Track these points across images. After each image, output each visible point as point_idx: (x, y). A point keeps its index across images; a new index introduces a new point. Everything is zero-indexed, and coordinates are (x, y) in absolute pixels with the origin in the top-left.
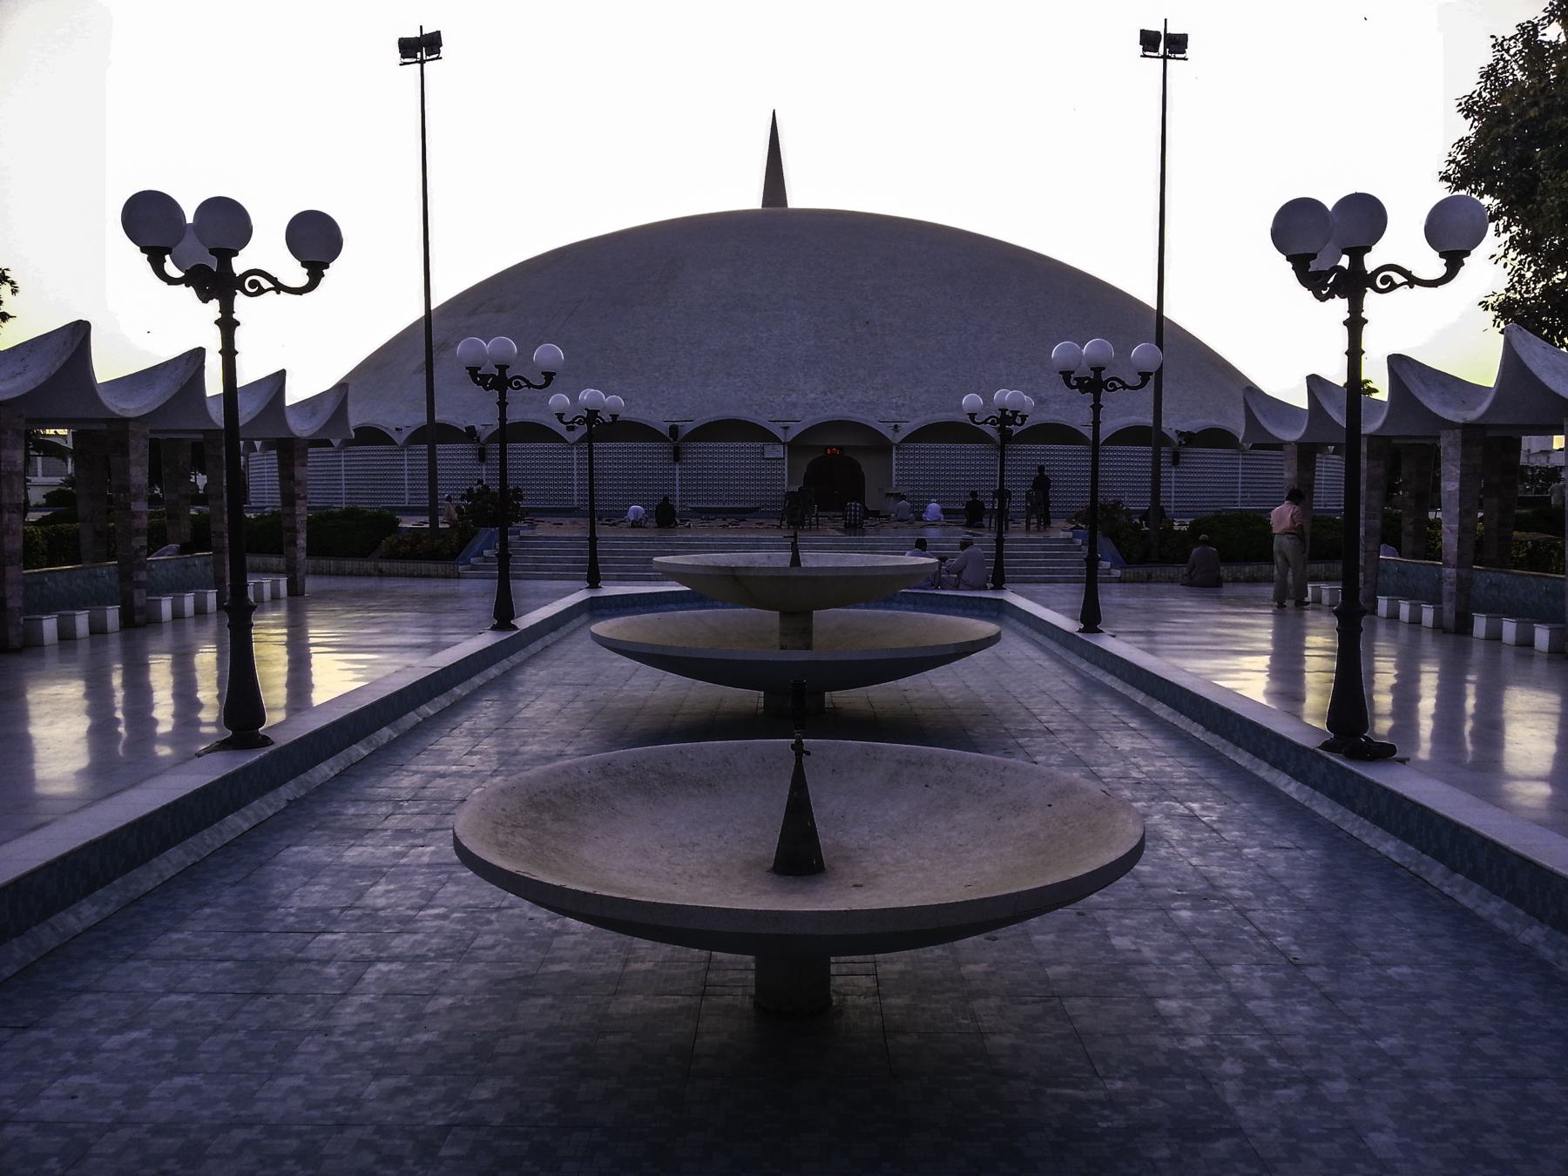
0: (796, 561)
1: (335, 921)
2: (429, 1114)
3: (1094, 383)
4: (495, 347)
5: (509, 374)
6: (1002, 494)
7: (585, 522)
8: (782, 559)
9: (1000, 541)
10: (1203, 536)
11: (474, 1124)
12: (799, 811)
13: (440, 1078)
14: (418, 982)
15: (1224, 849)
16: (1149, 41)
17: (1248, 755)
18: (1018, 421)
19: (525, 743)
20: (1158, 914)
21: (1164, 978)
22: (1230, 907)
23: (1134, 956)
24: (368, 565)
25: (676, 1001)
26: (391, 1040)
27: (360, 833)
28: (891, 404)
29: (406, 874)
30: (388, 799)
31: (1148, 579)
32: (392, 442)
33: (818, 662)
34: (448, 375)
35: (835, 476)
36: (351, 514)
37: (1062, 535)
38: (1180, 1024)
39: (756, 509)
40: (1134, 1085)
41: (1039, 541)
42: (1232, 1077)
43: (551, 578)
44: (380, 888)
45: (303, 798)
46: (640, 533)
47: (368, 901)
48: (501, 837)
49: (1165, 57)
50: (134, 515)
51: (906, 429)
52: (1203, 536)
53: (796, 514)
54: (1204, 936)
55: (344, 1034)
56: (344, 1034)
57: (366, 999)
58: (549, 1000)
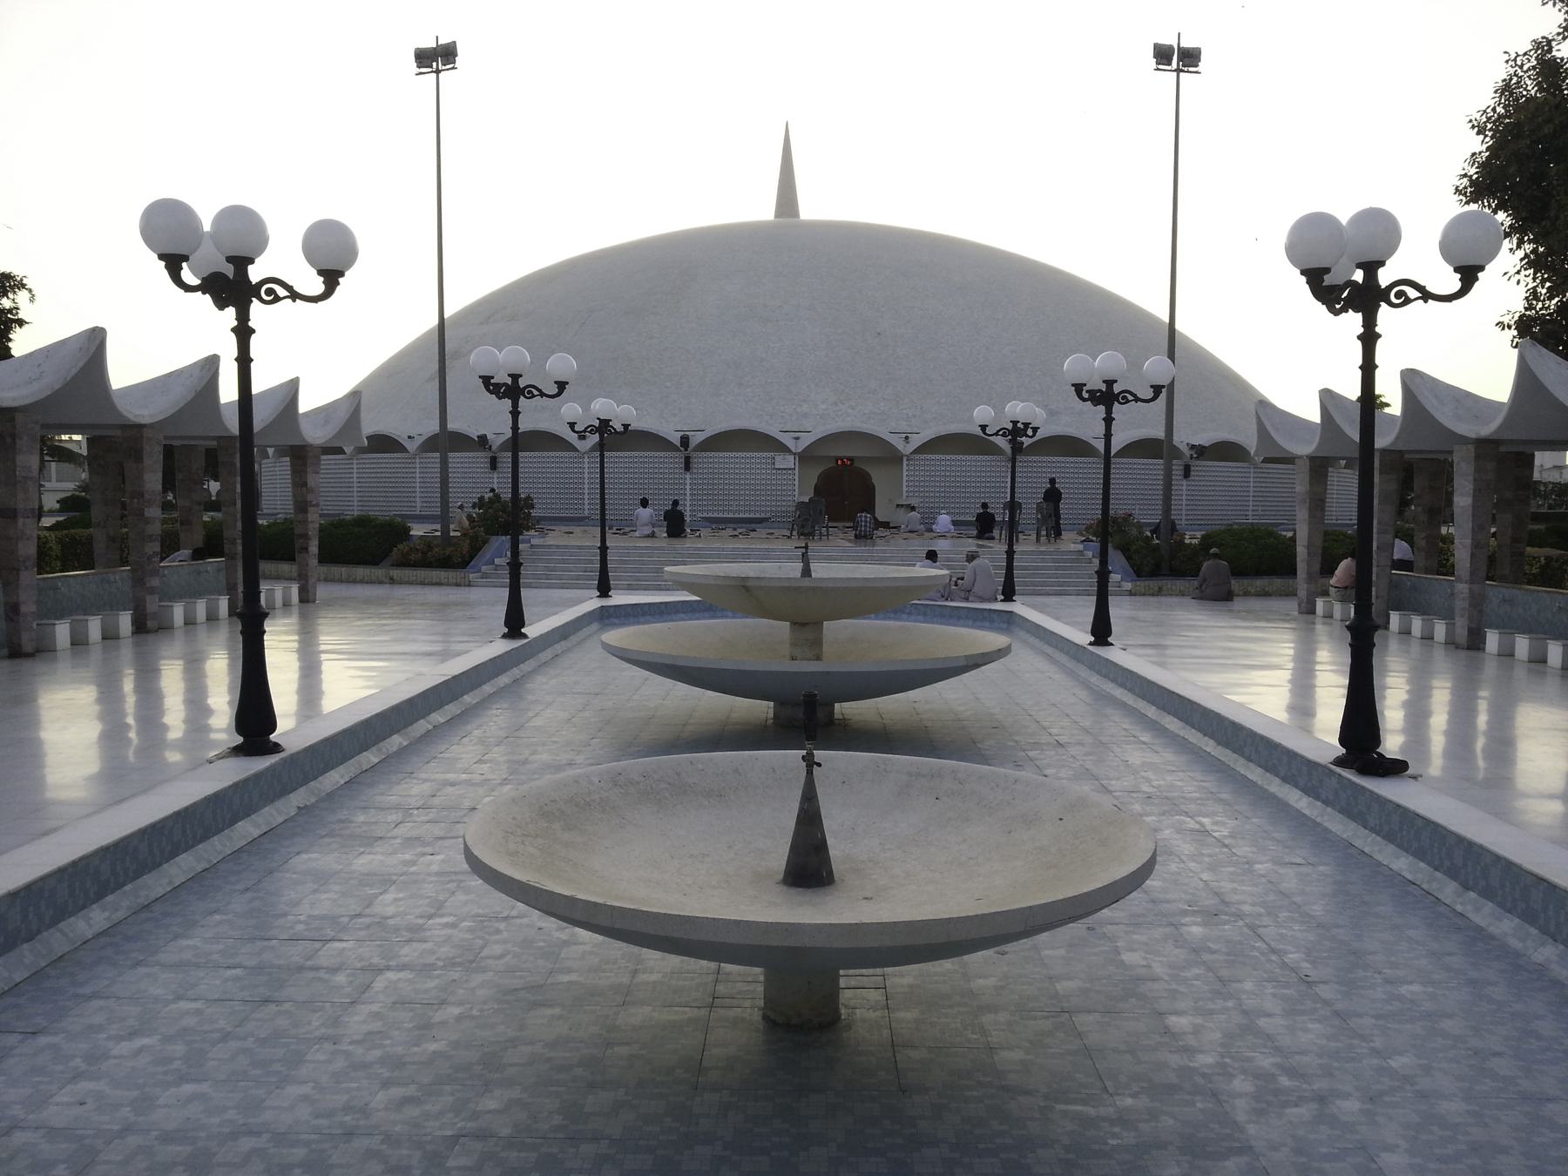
0: (806, 572)
4: (505, 359)
5: (522, 383)
6: (1013, 506)
8: (793, 569)
9: (1010, 554)
10: (1213, 550)
11: (481, 1135)
13: (448, 1088)
16: (1162, 55)
18: (1030, 432)
19: (535, 752)
22: (1241, 923)
23: (1142, 971)
24: (378, 572)
26: (400, 1050)
27: (370, 841)
29: (415, 882)
30: (397, 808)
32: (404, 450)
35: (842, 489)
36: (362, 522)
37: (1073, 547)
40: (1143, 1102)
42: (1240, 1095)
44: (389, 897)
45: (313, 805)
47: (377, 909)
49: (1178, 71)
52: (1213, 550)
57: (375, 1008)
58: (557, 1011)
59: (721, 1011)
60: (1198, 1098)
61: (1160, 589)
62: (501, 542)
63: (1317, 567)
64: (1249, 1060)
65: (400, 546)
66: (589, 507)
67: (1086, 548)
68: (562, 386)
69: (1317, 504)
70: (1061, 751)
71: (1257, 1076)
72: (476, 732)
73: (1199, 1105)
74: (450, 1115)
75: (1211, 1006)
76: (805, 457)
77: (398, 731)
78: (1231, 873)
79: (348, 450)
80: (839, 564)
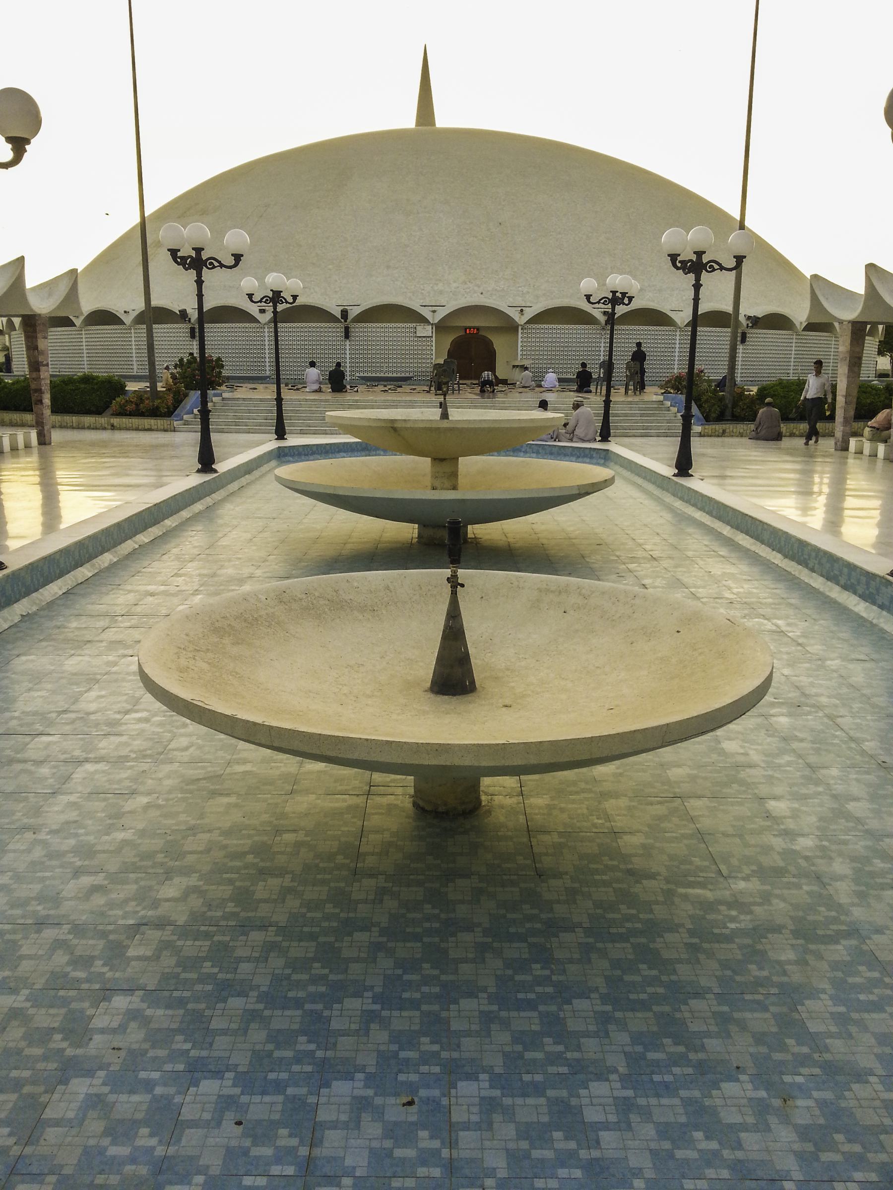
0: (445, 416)
1: (51, 723)
2: (120, 913)
3: (696, 266)
4: (191, 234)
5: (205, 256)
6: (609, 366)
7: (274, 387)
9: (607, 403)
10: (768, 400)
11: (160, 924)
12: (454, 632)
13: (132, 876)
14: (120, 781)
15: (810, 661)
17: (821, 580)
18: (626, 301)
19: (222, 567)
20: (759, 720)
21: (770, 780)
22: (821, 714)
23: (741, 759)
24: (102, 420)
25: (344, 800)
26: (91, 838)
27: (80, 644)
28: (517, 293)
29: (116, 681)
30: (106, 615)
31: (723, 434)
32: (122, 323)
33: (463, 501)
34: (161, 262)
35: (471, 354)
36: (87, 379)
37: (654, 398)
38: (791, 824)
39: (409, 378)
40: (754, 885)
41: (637, 403)
42: (842, 878)
43: (248, 432)
44: (93, 694)
45: (35, 614)
46: (322, 396)
47: (83, 705)
48: (183, 662)
51: (529, 314)
52: (768, 400)
53: (441, 381)
54: (802, 740)
55: (51, 832)
56: (51, 832)
57: (72, 798)
58: (233, 799)
59: (378, 799)
60: (803, 881)
61: (724, 431)
62: (195, 396)
63: (852, 413)
64: (845, 842)
65: (118, 399)
66: (269, 370)
67: (665, 399)
68: (238, 258)
69: (855, 361)
70: (655, 563)
71: (853, 859)
72: (175, 551)
73: (805, 888)
74: (134, 903)
75: (804, 791)
76: (441, 327)
77: (108, 550)
78: (808, 669)
79: (78, 322)
80: (469, 411)
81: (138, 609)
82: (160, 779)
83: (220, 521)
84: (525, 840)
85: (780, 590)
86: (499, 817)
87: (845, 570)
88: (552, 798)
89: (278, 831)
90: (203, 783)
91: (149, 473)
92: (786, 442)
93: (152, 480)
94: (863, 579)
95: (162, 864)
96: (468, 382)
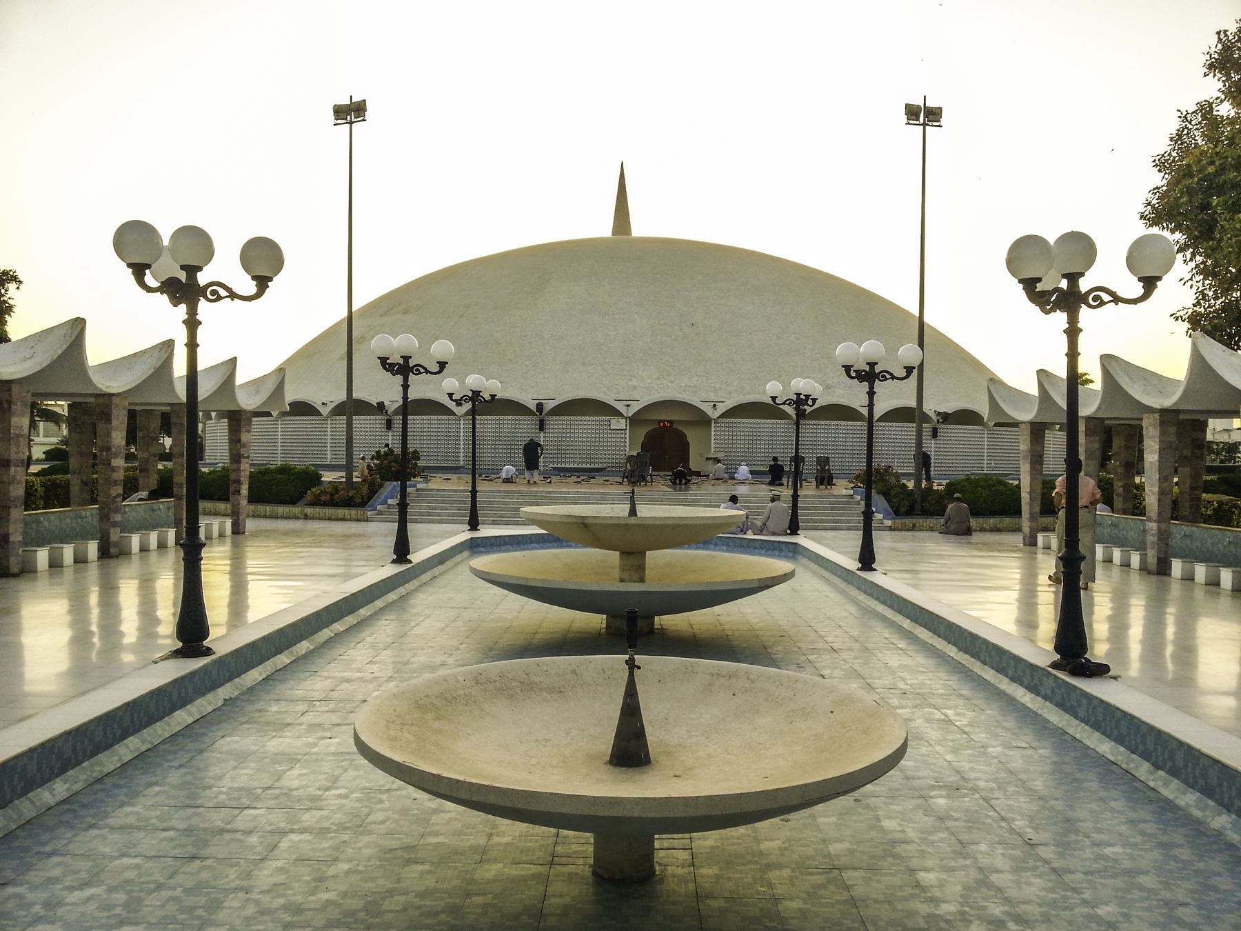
0: (633, 512)
1: (258, 798)
4: (398, 343)
5: (411, 363)
9: (795, 497)
12: (631, 709)
14: (323, 850)
15: (973, 748)
16: (912, 113)
18: (810, 402)
21: (923, 854)
22: (977, 796)
23: (898, 836)
24: (296, 510)
25: (529, 869)
26: (299, 899)
28: (711, 390)
29: (316, 760)
30: (304, 700)
31: (913, 528)
32: (318, 413)
35: (666, 446)
36: (284, 470)
37: (844, 492)
38: (937, 893)
39: (603, 469)
44: (295, 772)
45: (237, 698)
47: (285, 782)
48: (392, 733)
49: (924, 125)
50: (113, 470)
51: (722, 408)
54: (956, 820)
55: (262, 892)
56: (262, 892)
57: (280, 864)
58: (426, 867)
61: (914, 525)
62: (392, 486)
66: (463, 459)
68: (442, 365)
70: (835, 655)
75: (953, 864)
76: (635, 421)
80: (660, 506)
81: (335, 695)
82: (360, 849)
83: (413, 611)
84: (694, 904)
85: (953, 681)
86: (671, 885)
87: (1012, 663)
88: (721, 869)
89: (468, 895)
90: (399, 853)
91: (340, 563)
92: (976, 537)
93: (340, 570)
94: (1028, 671)
95: (363, 921)
96: (662, 473)
